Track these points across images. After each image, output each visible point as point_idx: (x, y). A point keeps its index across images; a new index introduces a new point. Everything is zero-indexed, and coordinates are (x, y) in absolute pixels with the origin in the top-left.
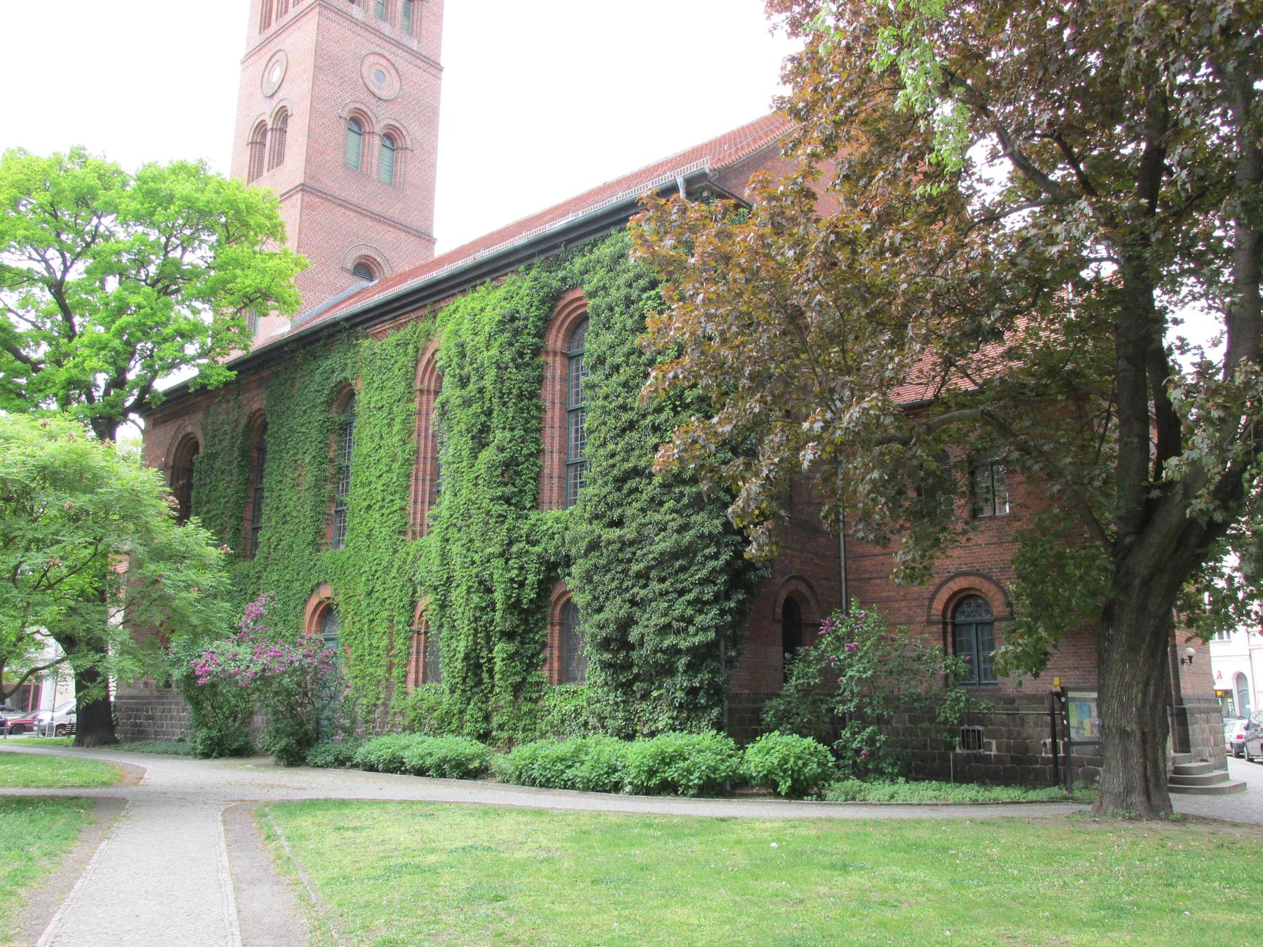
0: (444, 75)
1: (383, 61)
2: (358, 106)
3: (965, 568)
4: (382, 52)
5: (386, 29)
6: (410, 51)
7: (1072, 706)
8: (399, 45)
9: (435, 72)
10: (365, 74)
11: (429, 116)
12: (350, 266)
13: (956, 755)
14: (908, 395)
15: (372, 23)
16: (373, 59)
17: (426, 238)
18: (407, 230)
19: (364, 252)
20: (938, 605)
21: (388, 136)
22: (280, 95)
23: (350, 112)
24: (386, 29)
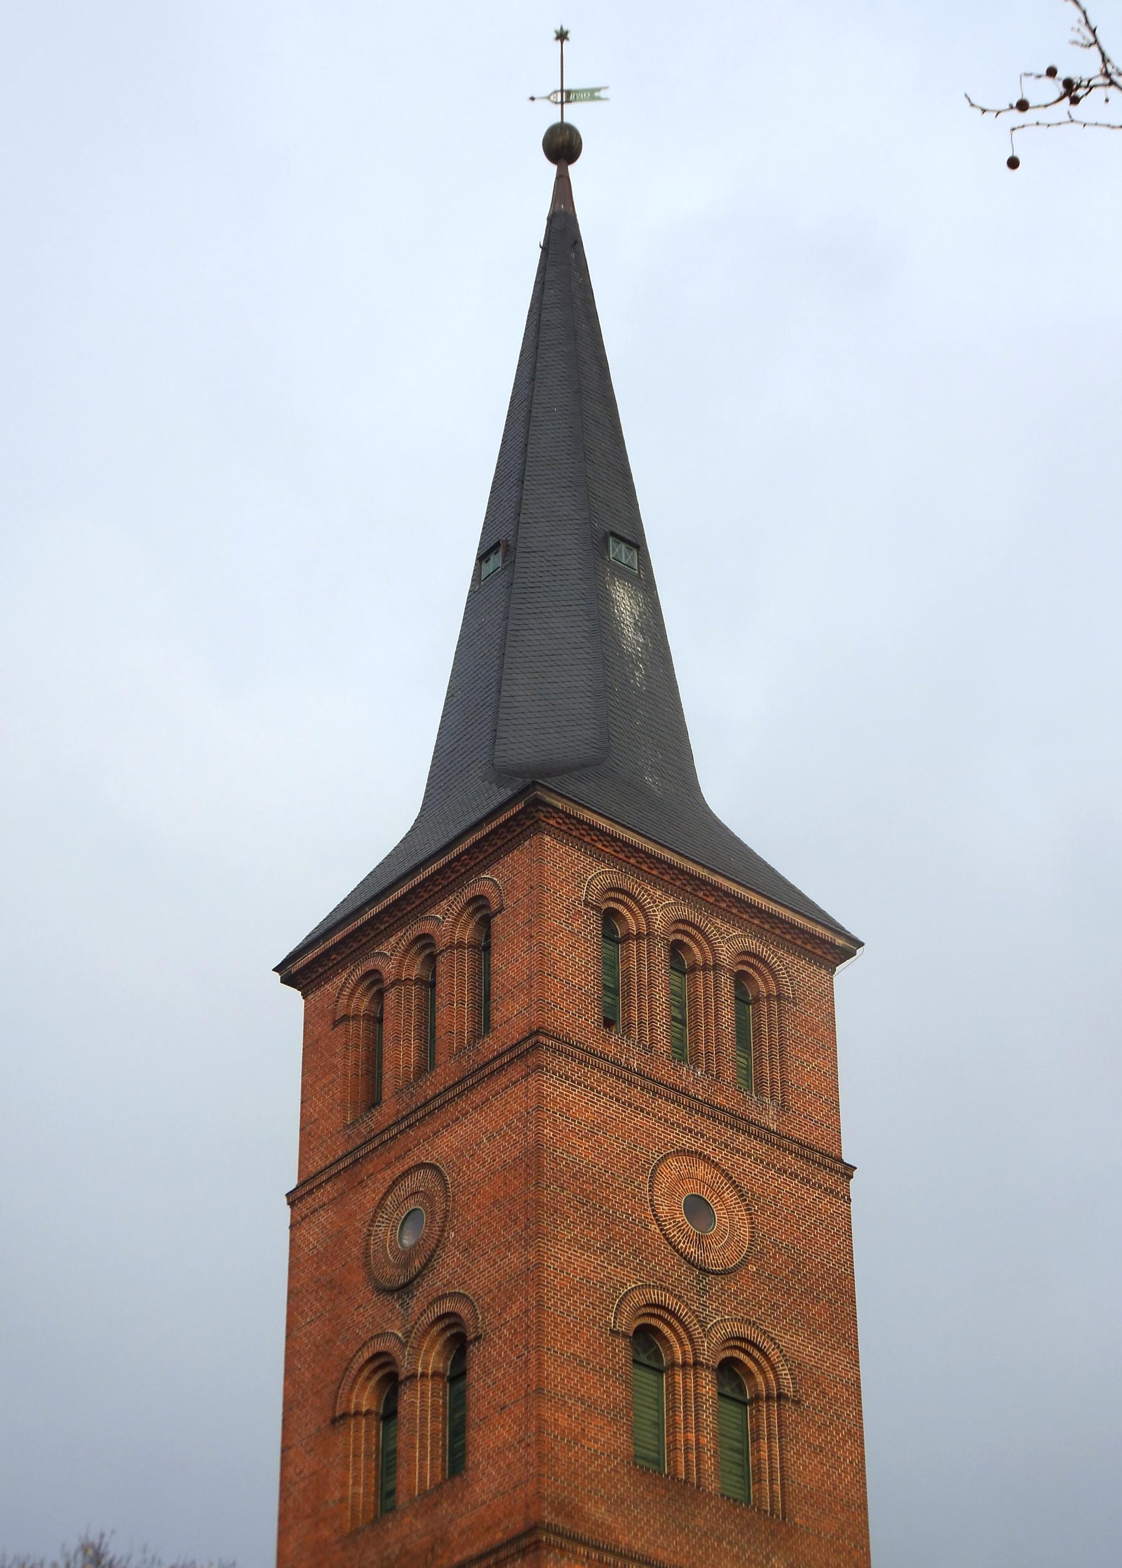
0: (856, 1185)
1: (702, 1170)
2: (655, 1296)
4: (697, 1145)
5: (688, 1077)
6: (763, 1134)
8: (741, 1123)
9: (829, 1180)
10: (663, 1210)
14: (394, 938)
15: (664, 1073)
16: (675, 1167)
22: (435, 1282)
23: (636, 1313)
24: (688, 1077)
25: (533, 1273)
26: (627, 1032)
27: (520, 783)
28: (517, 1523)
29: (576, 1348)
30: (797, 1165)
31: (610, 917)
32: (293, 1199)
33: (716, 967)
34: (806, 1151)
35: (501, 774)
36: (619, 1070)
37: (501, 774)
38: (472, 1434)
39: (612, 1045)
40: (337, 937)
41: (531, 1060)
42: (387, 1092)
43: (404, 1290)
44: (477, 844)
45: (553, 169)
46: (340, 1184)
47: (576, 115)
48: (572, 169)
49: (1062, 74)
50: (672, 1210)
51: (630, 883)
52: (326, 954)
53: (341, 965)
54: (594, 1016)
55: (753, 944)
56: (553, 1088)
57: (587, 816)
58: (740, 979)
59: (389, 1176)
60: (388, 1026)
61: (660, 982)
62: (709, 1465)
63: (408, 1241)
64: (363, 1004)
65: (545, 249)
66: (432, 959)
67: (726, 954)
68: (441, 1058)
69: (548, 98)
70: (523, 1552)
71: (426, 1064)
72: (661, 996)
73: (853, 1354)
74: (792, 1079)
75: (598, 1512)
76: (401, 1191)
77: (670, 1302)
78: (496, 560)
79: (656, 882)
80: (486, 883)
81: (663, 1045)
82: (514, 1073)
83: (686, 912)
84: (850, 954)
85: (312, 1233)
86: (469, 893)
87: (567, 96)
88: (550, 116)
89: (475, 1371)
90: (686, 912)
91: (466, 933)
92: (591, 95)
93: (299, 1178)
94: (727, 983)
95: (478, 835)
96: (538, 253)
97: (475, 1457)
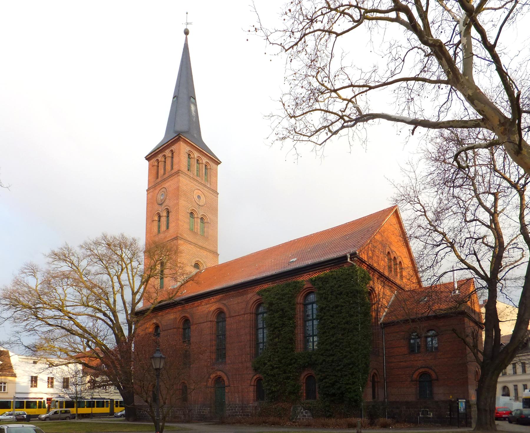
1: (200, 192)
2: (193, 208)
3: (423, 366)
4: (199, 188)
5: (198, 179)
7: (459, 403)
8: (205, 186)
9: (216, 195)
10: (194, 197)
11: (214, 210)
12: (193, 265)
13: (420, 417)
15: (195, 178)
17: (216, 254)
18: (210, 251)
19: (197, 259)
20: (415, 376)
21: (202, 218)
22: (165, 204)
24: (198, 179)
25: (177, 204)
26: (191, 172)
27: (178, 134)
28: (175, 236)
29: (183, 214)
30: (212, 192)
31: (189, 155)
32: (147, 191)
33: (203, 163)
34: (213, 190)
35: (175, 132)
36: (189, 177)
37: (175, 132)
38: (170, 224)
39: (189, 173)
40: (153, 154)
41: (178, 174)
42: (159, 177)
43: (161, 204)
44: (172, 142)
45: (185, 36)
46: (153, 189)
47: (189, 27)
48: (188, 36)
49: (255, 27)
50: (196, 197)
51: (192, 150)
52: (151, 156)
53: (153, 158)
54: (186, 169)
55: (208, 161)
56: (181, 178)
57: (187, 140)
58: (206, 165)
59: (160, 188)
60: (159, 167)
61: (195, 165)
62: (199, 230)
63: (162, 198)
64: (156, 164)
65: (184, 49)
66: (165, 158)
67: (204, 162)
68: (166, 173)
69: (35, 276)
70: (176, 240)
71: (164, 174)
72: (195, 167)
73: (217, 218)
74: (212, 180)
75: (185, 235)
76: (161, 191)
77: (195, 209)
78: (175, 98)
79: (195, 150)
80: (173, 148)
81: (195, 174)
82: (176, 176)
83: (199, 155)
84: (220, 164)
85: (149, 195)
86: (170, 149)
87: (187, 24)
88: (184, 27)
89: (170, 216)
90: (199, 155)
91: (170, 155)
92: (191, 23)
93: (148, 185)
94: (204, 166)
95: (172, 141)
96: (183, 50)
97: (170, 227)
